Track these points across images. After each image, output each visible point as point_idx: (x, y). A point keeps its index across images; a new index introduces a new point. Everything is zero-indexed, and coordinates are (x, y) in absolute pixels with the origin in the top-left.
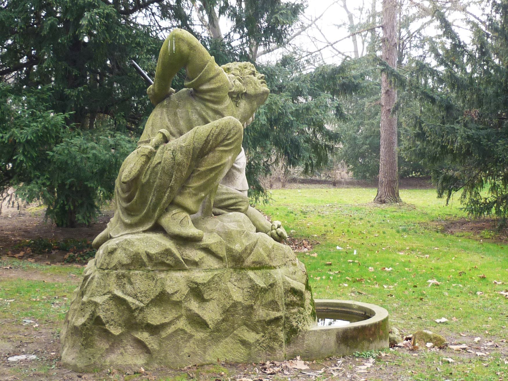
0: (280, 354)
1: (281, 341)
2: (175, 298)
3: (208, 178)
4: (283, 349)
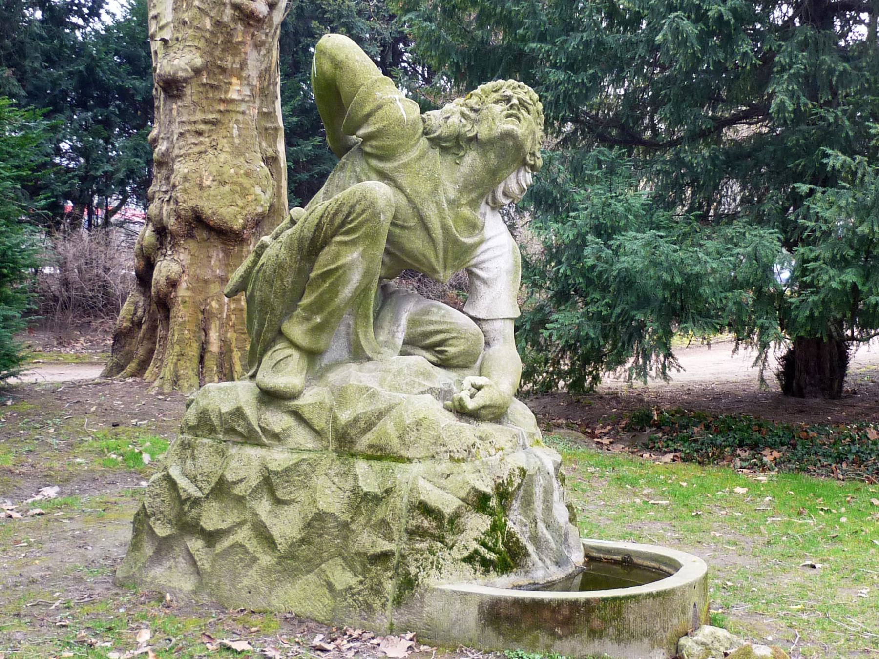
0: (381, 620)
1: (385, 597)
2: (238, 490)
3: (321, 290)
4: (388, 613)
